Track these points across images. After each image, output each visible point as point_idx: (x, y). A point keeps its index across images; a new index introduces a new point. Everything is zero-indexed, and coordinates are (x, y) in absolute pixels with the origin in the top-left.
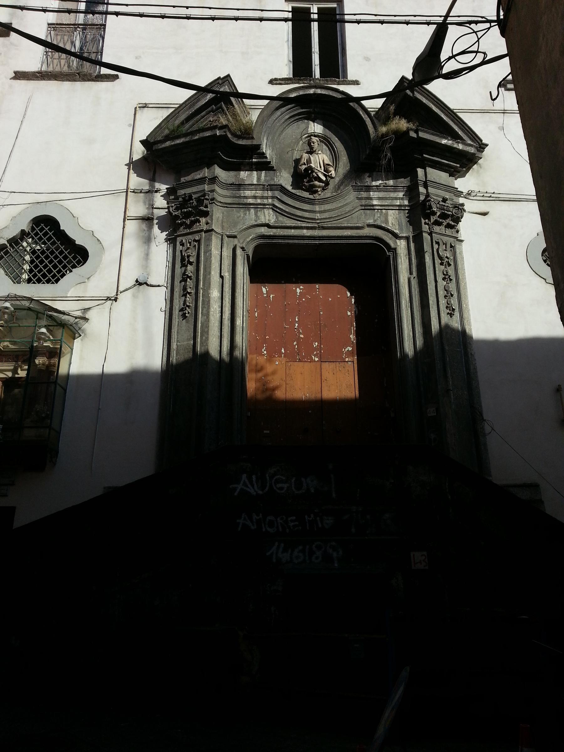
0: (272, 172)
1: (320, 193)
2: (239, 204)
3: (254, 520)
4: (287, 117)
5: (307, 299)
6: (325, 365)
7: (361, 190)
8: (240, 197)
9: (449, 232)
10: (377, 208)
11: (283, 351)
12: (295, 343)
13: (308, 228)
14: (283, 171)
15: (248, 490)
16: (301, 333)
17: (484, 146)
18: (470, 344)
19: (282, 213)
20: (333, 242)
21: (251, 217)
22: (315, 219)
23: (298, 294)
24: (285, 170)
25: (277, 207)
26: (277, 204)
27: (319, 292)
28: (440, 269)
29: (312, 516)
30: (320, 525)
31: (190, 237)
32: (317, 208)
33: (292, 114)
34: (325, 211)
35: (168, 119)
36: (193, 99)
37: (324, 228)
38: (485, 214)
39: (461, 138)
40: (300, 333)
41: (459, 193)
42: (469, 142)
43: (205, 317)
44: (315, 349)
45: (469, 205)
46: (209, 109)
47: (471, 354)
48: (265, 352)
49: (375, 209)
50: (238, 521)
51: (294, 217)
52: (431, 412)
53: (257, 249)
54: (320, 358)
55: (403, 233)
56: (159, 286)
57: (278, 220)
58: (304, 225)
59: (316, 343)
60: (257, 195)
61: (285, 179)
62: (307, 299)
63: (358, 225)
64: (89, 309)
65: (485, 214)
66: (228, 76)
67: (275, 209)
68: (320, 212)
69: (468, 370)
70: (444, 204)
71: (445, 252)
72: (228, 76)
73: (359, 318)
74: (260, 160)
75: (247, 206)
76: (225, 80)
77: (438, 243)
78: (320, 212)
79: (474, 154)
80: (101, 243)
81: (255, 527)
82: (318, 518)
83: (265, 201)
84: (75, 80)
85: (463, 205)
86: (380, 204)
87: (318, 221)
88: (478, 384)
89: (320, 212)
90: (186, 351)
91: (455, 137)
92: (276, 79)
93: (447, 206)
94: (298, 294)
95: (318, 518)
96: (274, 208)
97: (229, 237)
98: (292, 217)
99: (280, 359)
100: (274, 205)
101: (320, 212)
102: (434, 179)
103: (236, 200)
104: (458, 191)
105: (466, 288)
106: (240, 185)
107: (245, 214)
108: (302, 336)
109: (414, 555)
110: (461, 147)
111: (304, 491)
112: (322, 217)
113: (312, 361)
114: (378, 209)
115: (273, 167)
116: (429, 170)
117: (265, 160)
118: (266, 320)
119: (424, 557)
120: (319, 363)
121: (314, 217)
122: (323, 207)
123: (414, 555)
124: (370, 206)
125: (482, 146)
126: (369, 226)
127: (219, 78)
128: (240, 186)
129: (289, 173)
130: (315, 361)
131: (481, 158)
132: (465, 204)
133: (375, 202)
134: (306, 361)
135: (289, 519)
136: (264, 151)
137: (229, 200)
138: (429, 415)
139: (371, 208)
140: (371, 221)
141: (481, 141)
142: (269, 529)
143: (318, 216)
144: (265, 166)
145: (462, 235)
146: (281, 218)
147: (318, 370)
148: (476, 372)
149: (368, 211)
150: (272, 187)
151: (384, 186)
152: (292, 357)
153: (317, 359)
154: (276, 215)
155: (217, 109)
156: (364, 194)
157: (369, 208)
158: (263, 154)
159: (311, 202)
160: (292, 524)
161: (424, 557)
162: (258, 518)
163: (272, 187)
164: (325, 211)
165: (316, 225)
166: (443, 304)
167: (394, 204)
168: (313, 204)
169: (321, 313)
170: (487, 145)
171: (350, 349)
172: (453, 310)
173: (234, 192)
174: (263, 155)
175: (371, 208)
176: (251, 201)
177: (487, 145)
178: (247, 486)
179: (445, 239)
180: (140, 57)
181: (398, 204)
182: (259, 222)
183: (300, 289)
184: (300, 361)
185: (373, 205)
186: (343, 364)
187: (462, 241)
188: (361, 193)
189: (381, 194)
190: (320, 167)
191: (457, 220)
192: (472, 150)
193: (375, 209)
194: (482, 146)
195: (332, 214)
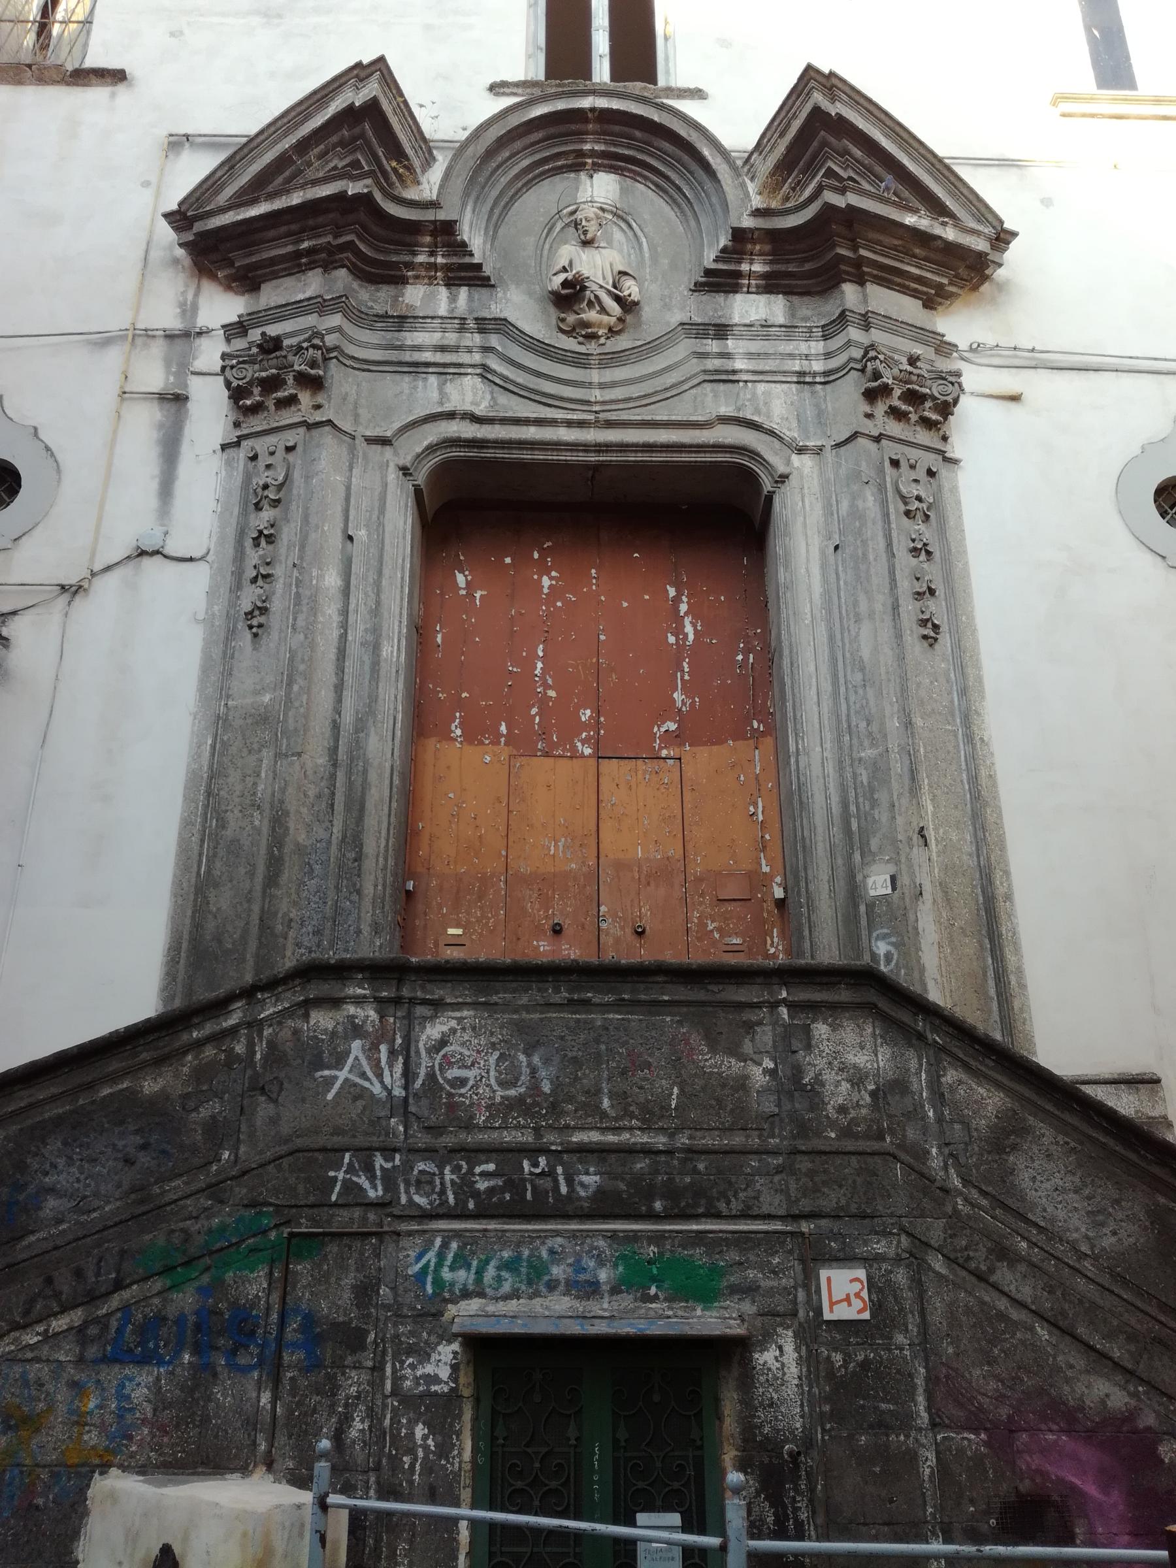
0: (484, 291)
1: (602, 340)
2: (400, 363)
3: (378, 1173)
4: (526, 163)
5: (566, 602)
6: (608, 767)
7: (705, 336)
8: (400, 348)
9: (924, 437)
10: (745, 377)
11: (503, 729)
12: (534, 711)
13: (569, 424)
14: (513, 287)
15: (366, 1084)
16: (550, 687)
17: (1007, 237)
18: (979, 714)
19: (507, 387)
20: (632, 458)
21: (428, 394)
22: (588, 403)
23: (546, 591)
24: (518, 285)
25: (494, 372)
26: (494, 364)
27: (598, 586)
28: (899, 523)
29: (542, 1161)
30: (564, 1189)
31: (271, 440)
32: (595, 376)
33: (538, 157)
34: (613, 385)
35: (233, 162)
36: (293, 114)
37: (610, 424)
38: (1015, 398)
39: (952, 216)
40: (547, 686)
41: (944, 348)
42: (972, 224)
43: (302, 636)
44: (585, 726)
45: (973, 378)
46: (334, 139)
47: (982, 739)
48: (459, 732)
49: (738, 381)
50: (332, 1174)
51: (537, 398)
52: (877, 884)
53: (443, 471)
54: (597, 747)
55: (808, 438)
56: (191, 559)
57: (496, 404)
58: (559, 415)
59: (588, 712)
60: (446, 342)
61: (519, 305)
62: (566, 602)
63: (695, 418)
64: (14, 613)
65: (1015, 398)
66: (382, 59)
67: (489, 376)
68: (602, 385)
69: (974, 779)
70: (909, 368)
71: (914, 485)
72: (382, 59)
73: (1115, 1112)
74: (455, 260)
75: (417, 368)
76: (373, 68)
77: (895, 463)
78: (602, 386)
79: (981, 255)
80: (52, 455)
81: (380, 1193)
82: (560, 1170)
83: (465, 358)
84: (20, 82)
85: (958, 374)
86: (751, 368)
87: (597, 408)
88: (1000, 816)
89: (602, 386)
90: (249, 721)
91: (938, 209)
92: (504, 84)
93: (918, 376)
94: (546, 591)
95: (560, 1170)
96: (485, 372)
97: (371, 441)
98: (532, 396)
99: (495, 748)
100: (484, 367)
101: (602, 385)
102: (886, 310)
103: (393, 355)
104: (946, 343)
105: (966, 575)
106: (403, 318)
107: (415, 388)
108: (552, 693)
109: (829, 1279)
110: (950, 234)
111: (522, 1090)
112: (607, 398)
113: (575, 755)
114: (746, 382)
115: (488, 279)
116: (871, 288)
117: (467, 260)
118: (463, 653)
119: (857, 1286)
120: (592, 762)
121: (586, 398)
122: (610, 375)
123: (829, 1279)
124: (727, 372)
125: (1002, 238)
126: (725, 420)
127: (359, 65)
128: (402, 321)
129: (530, 294)
130: (582, 756)
131: (1000, 265)
132: (964, 374)
133: (739, 364)
134: (560, 756)
135: (478, 1170)
136: (466, 238)
137: (378, 355)
138: (872, 893)
139: (726, 378)
140: (725, 410)
141: (1002, 222)
142: (417, 1199)
143: (596, 395)
144: (467, 275)
145: (956, 448)
146: (504, 399)
147: (592, 778)
148: (995, 785)
149: (722, 387)
150: (484, 325)
151: (763, 326)
152: (524, 744)
153: (588, 751)
154: (492, 393)
155: (354, 139)
156: (713, 346)
157: (724, 377)
158: (464, 244)
159: (579, 361)
160: (482, 1185)
161: (857, 1286)
162: (388, 1165)
163: (484, 325)
164: (613, 385)
165: (591, 417)
166: (909, 612)
167: (786, 368)
168: (585, 366)
169: (602, 637)
170: (1014, 234)
171: (673, 726)
172: (936, 627)
173: (389, 335)
174: (462, 248)
175: (726, 378)
176: (428, 356)
177: (1014, 234)
178: (368, 1079)
179: (914, 454)
180: (181, 33)
181: (797, 368)
182: (448, 407)
183: (551, 578)
184: (547, 755)
185: (734, 372)
186: (652, 765)
187: (954, 462)
188: (705, 341)
189: (755, 346)
190: (604, 278)
191: (946, 409)
192: (981, 245)
193: (738, 381)
194: (1002, 238)
195: (635, 391)
